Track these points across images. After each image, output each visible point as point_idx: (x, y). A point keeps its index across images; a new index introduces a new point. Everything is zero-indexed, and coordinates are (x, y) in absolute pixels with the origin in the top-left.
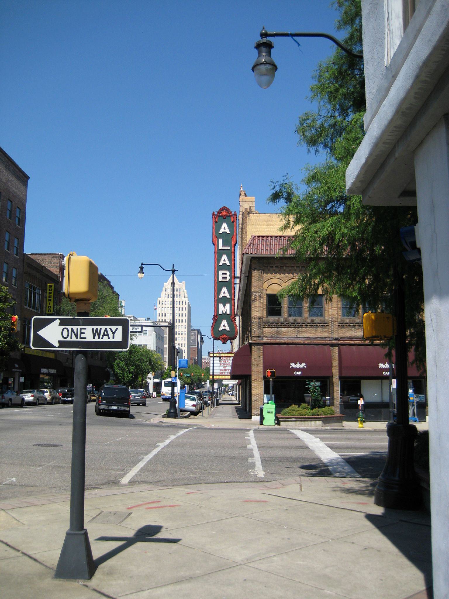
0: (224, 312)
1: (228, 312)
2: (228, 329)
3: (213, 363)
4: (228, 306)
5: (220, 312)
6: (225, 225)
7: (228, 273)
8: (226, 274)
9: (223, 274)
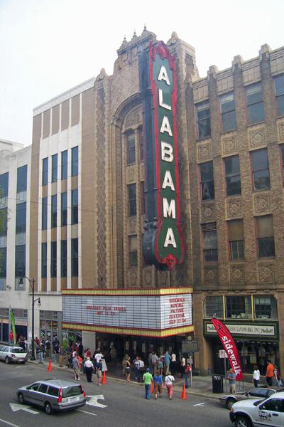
1: (174, 217)
3: (105, 326)
4: (173, 202)
5: (165, 216)
6: (163, 70)
7: (171, 150)
8: (168, 149)
9: (167, 149)
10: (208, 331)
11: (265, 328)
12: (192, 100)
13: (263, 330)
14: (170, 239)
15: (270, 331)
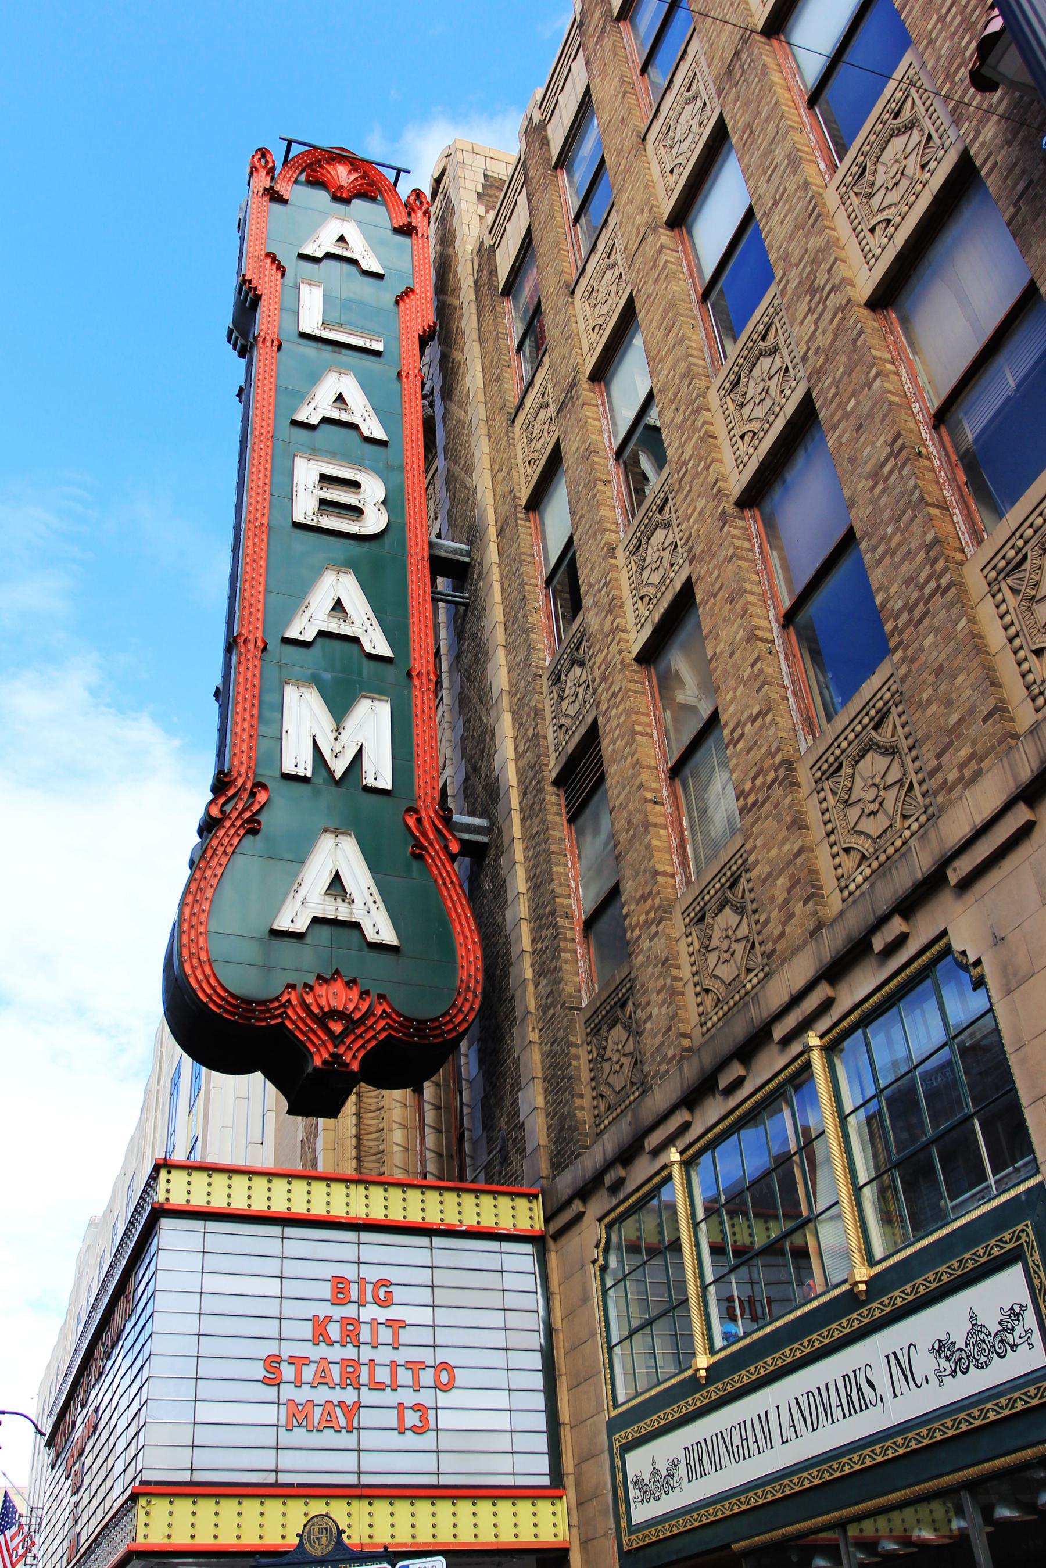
0: (339, 768)
1: (379, 771)
2: (380, 928)
10: (641, 1513)
11: (947, 1320)
12: (492, 285)
13: (942, 1348)
14: (334, 879)
15: (1002, 1344)
